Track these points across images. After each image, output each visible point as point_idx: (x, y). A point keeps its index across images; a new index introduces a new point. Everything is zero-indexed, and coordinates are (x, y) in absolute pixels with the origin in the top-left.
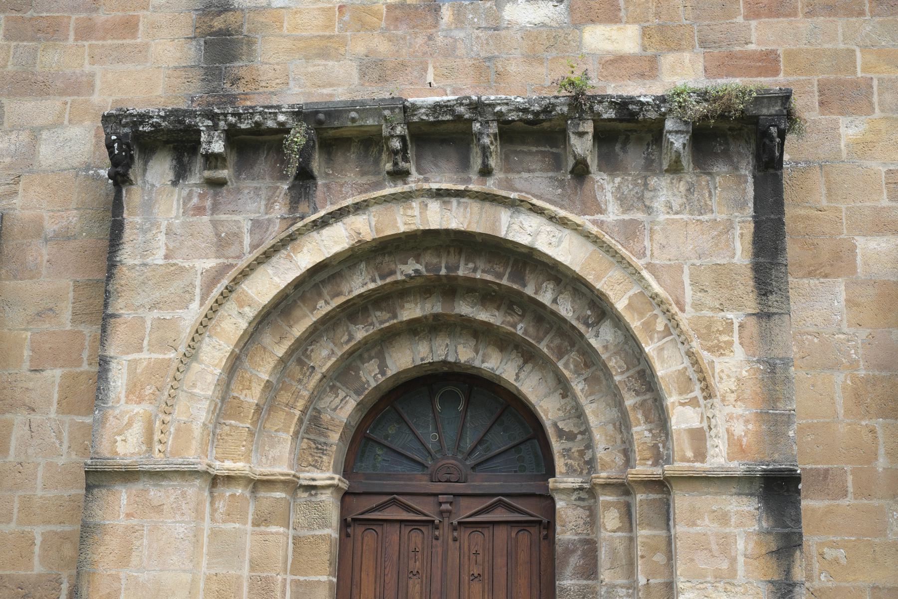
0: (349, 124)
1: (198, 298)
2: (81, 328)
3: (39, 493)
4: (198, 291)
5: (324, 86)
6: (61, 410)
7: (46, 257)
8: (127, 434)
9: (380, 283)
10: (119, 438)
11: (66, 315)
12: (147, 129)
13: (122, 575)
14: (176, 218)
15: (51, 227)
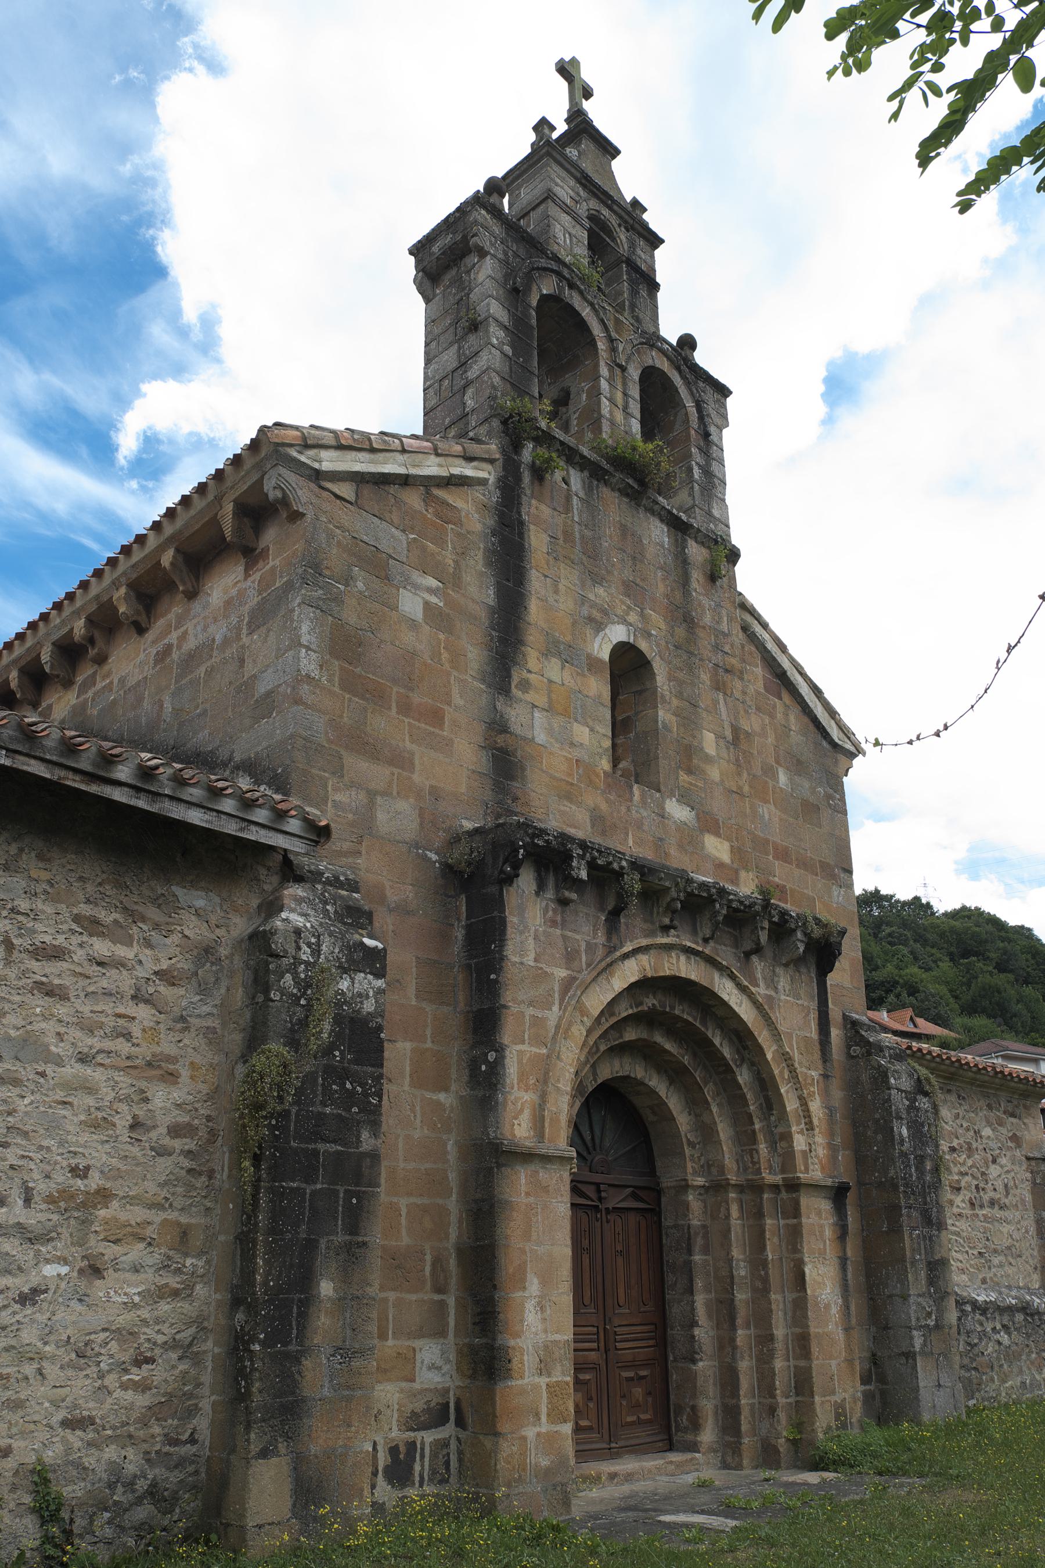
0: (657, 881)
1: (557, 1002)
2: (424, 1005)
3: (402, 1165)
4: (557, 995)
5: (571, 826)
6: (413, 1085)
7: (391, 927)
8: (521, 1117)
9: (635, 1010)
10: (516, 1122)
11: (412, 990)
12: (541, 843)
13: (527, 1249)
14: (540, 926)
15: (393, 897)
